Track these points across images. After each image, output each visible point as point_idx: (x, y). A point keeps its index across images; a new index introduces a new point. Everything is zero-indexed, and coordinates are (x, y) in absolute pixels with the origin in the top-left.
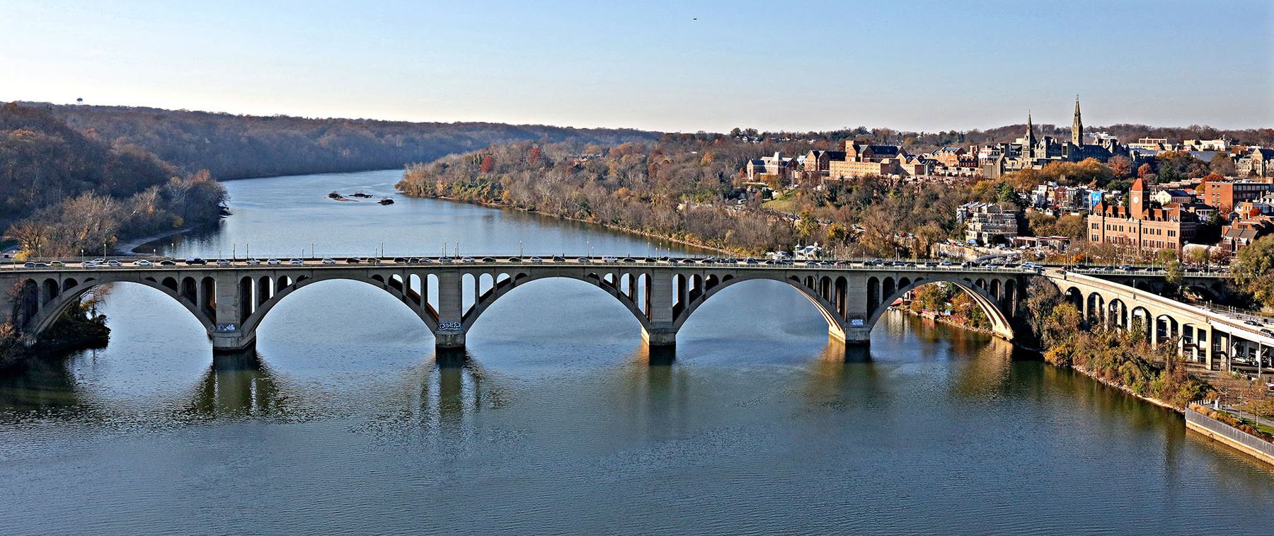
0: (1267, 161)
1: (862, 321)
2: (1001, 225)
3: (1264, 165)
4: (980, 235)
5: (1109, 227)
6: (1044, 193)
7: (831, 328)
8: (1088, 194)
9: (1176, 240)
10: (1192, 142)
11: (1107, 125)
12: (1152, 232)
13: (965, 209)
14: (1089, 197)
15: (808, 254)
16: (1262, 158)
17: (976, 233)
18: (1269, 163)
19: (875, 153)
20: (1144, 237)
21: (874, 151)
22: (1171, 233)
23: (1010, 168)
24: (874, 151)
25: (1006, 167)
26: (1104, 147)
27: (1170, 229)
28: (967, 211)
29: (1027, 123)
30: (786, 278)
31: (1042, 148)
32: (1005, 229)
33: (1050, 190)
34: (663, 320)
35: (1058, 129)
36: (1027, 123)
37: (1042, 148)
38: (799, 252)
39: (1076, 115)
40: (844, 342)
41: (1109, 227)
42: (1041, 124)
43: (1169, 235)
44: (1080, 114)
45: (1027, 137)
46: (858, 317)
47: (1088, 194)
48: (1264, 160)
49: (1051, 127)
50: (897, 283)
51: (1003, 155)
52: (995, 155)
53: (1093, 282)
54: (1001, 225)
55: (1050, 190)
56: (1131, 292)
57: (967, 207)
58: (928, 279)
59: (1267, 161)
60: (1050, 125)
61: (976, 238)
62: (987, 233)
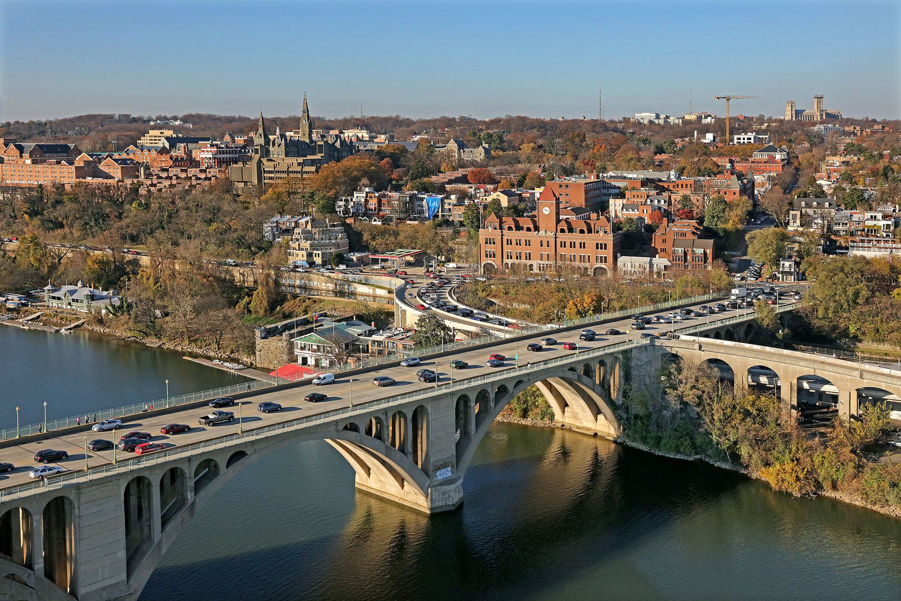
0: (461, 150)
1: (449, 469)
2: (333, 241)
3: (459, 154)
4: (310, 255)
5: (509, 242)
6: (363, 200)
7: (360, 477)
8: (422, 199)
9: (609, 253)
10: (337, 132)
11: (181, 114)
12: (572, 245)
14: (424, 203)
15: (71, 298)
17: (304, 253)
18: (464, 151)
19: (45, 152)
20: (507, 249)
22: (601, 246)
25: (266, 169)
26: (330, 142)
27: (600, 242)
28: (277, 226)
29: (259, 116)
30: (338, 431)
31: (279, 146)
32: (338, 246)
33: (371, 197)
36: (259, 116)
38: (51, 295)
39: (304, 112)
41: (509, 242)
42: (117, 114)
43: (597, 248)
44: (308, 111)
45: (261, 135)
46: (445, 466)
47: (422, 199)
48: (459, 150)
49: (127, 116)
50: (492, 396)
51: (258, 156)
52: (220, 154)
53: (734, 347)
55: (371, 197)
56: (857, 369)
57: (277, 222)
58: (529, 380)
59: (461, 150)
61: (305, 258)
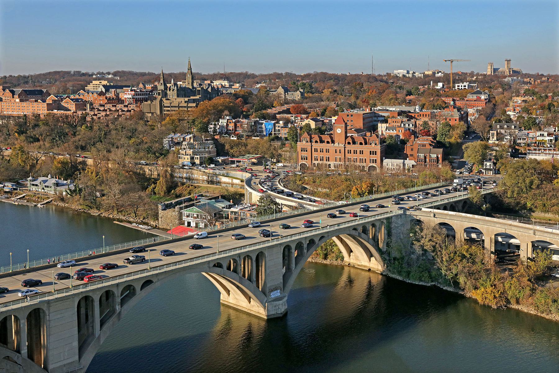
0: (286, 93)
1: (279, 291)
2: (207, 150)
4: (192, 158)
5: (316, 150)
6: (225, 124)
7: (224, 296)
8: (262, 124)
9: (378, 157)
10: (209, 82)
11: (112, 71)
12: (355, 152)
13: (171, 139)
14: (263, 126)
15: (44, 185)
16: (284, 91)
17: (189, 157)
18: (288, 94)
21: (27, 93)
22: (373, 153)
23: (169, 105)
24: (27, 93)
25: (165, 105)
26: (204, 88)
28: (172, 140)
30: (209, 267)
31: (173, 91)
32: (210, 152)
33: (230, 122)
34: (65, 362)
35: (83, 73)
37: (173, 91)
38: (32, 183)
39: (189, 70)
40: (266, 318)
41: (316, 150)
43: (371, 154)
44: (191, 69)
45: (162, 84)
46: (276, 289)
47: (262, 124)
48: (285, 93)
50: (305, 246)
51: (160, 97)
54: (207, 150)
55: (230, 122)
56: (531, 229)
57: (172, 138)
58: (328, 236)
59: (286, 93)
60: (78, 71)
61: (189, 160)
62: (198, 157)
